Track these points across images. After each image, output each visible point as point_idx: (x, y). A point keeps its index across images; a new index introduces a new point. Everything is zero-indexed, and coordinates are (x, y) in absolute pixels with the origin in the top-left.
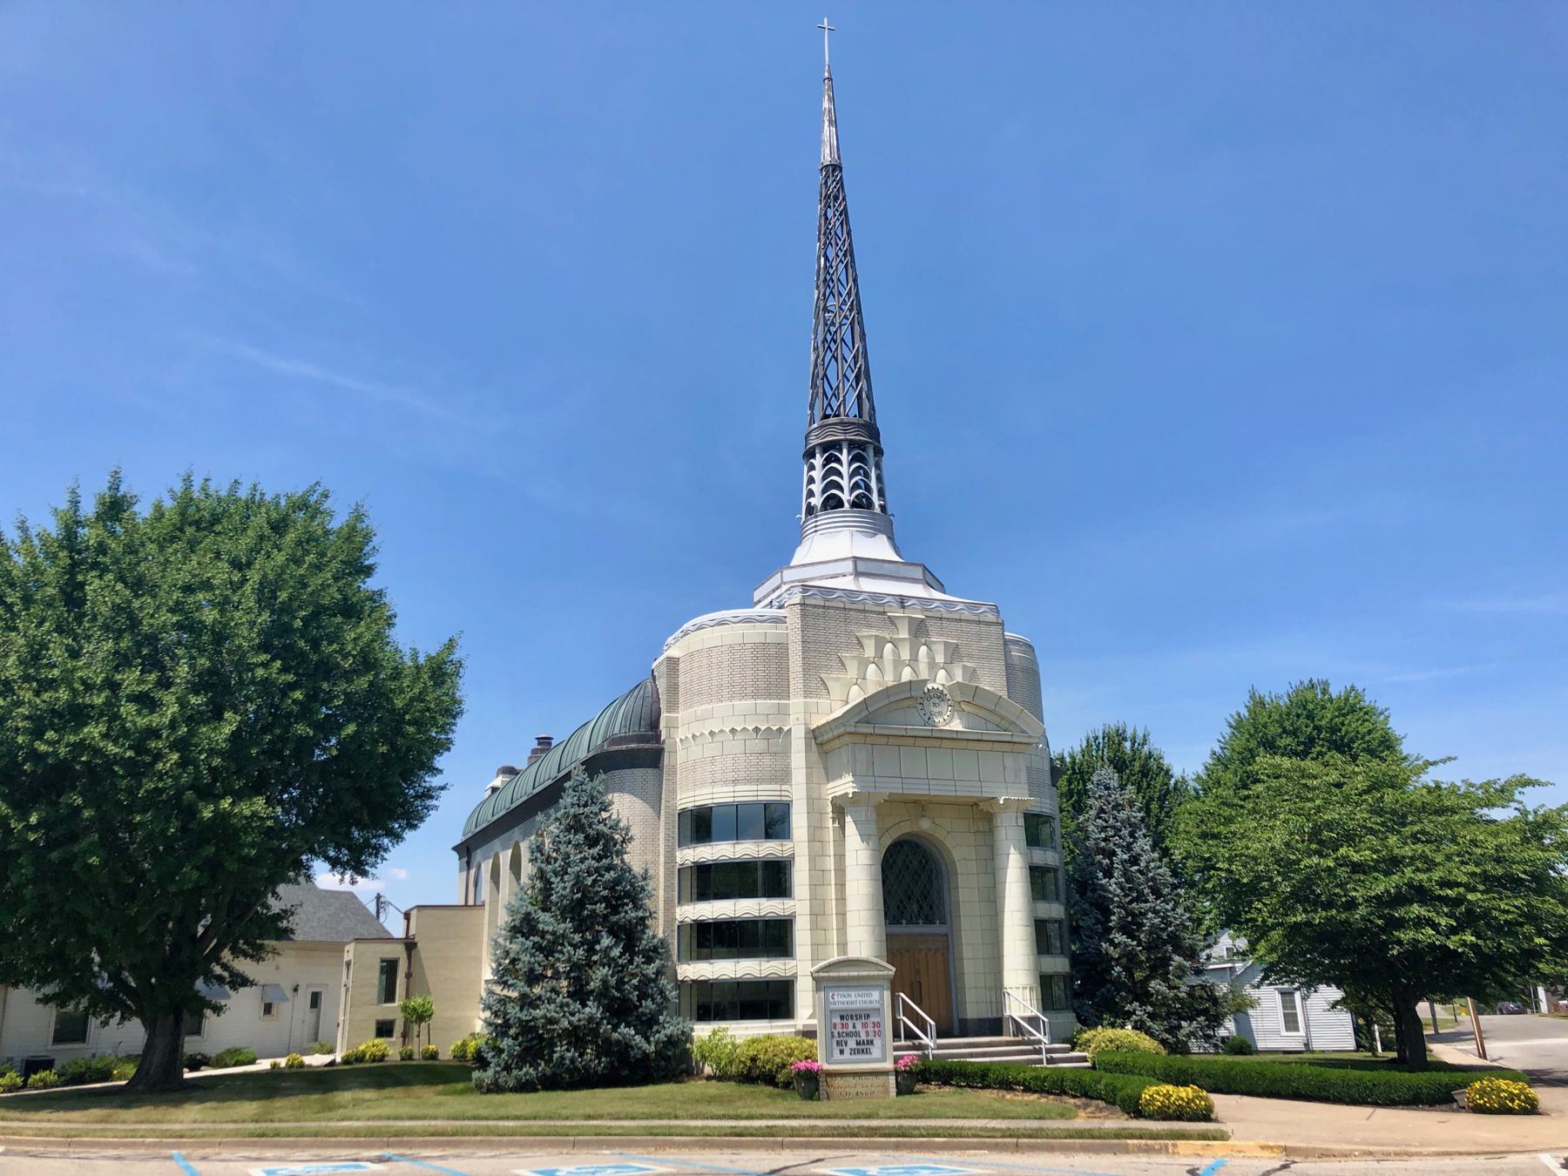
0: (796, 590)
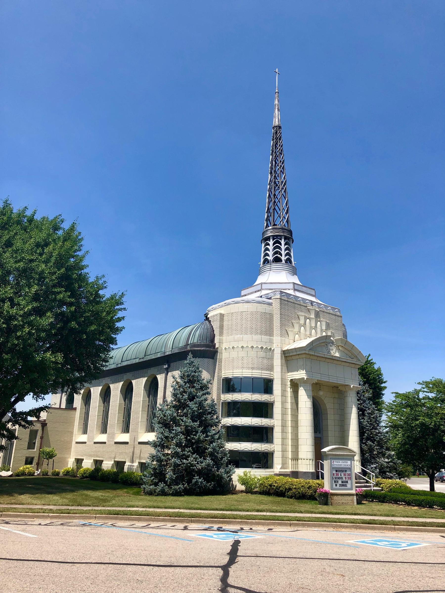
0: (277, 293)
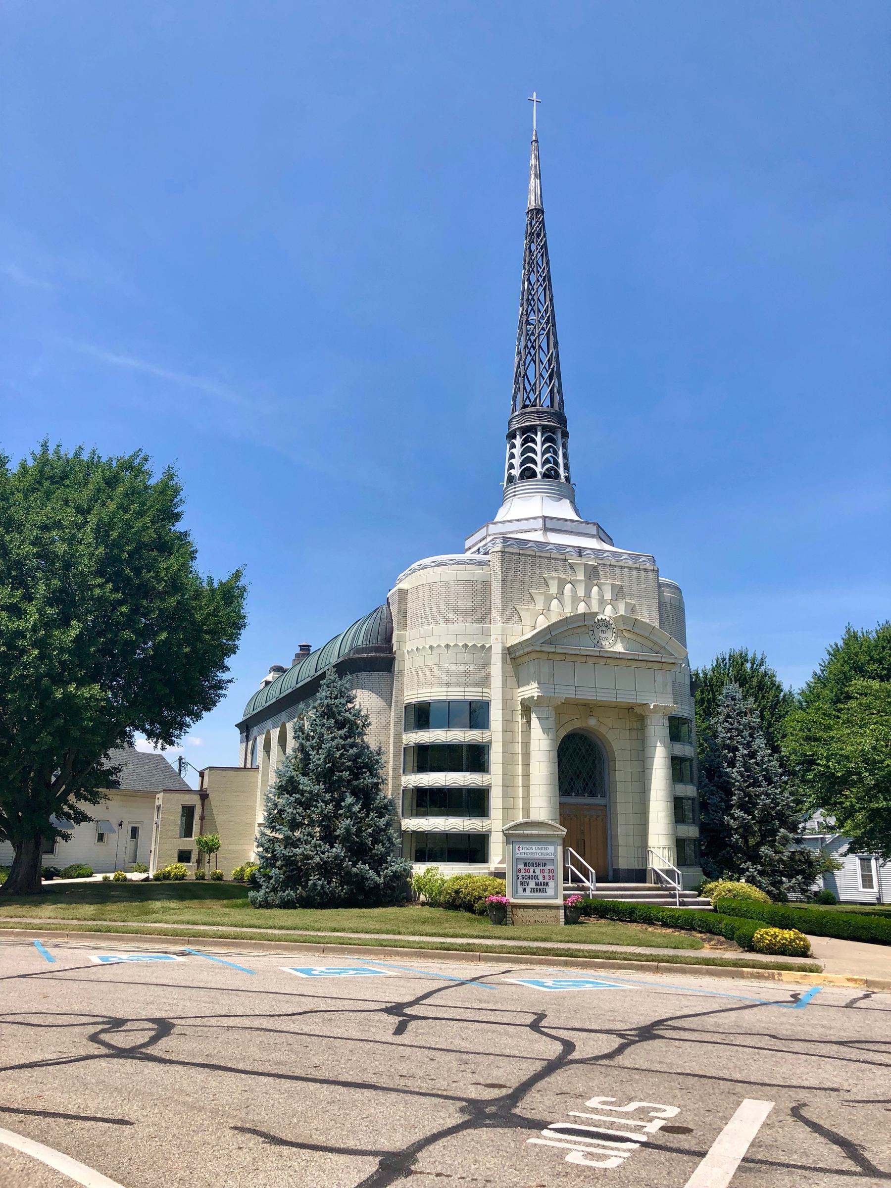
0: (498, 541)
